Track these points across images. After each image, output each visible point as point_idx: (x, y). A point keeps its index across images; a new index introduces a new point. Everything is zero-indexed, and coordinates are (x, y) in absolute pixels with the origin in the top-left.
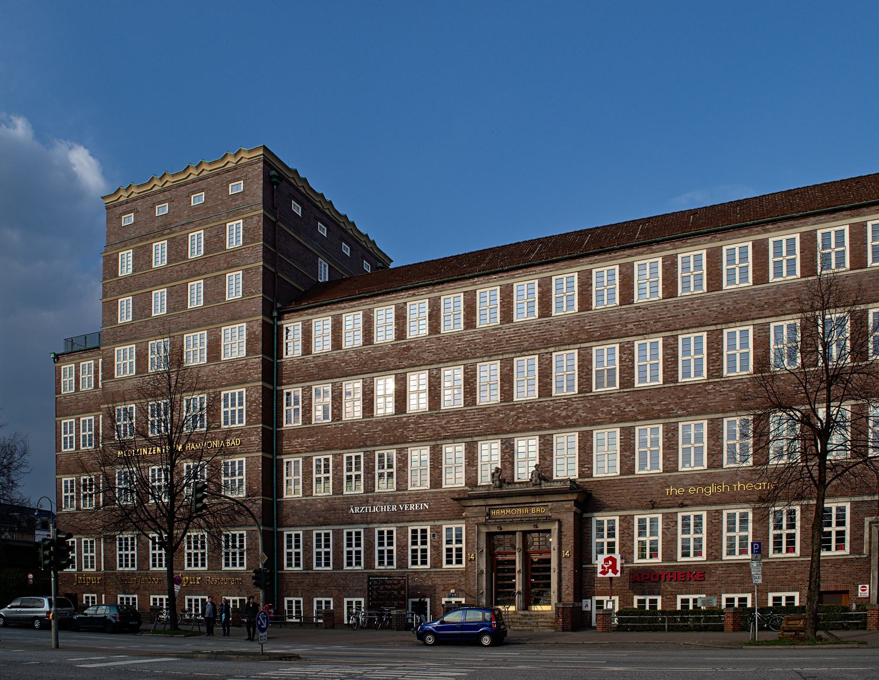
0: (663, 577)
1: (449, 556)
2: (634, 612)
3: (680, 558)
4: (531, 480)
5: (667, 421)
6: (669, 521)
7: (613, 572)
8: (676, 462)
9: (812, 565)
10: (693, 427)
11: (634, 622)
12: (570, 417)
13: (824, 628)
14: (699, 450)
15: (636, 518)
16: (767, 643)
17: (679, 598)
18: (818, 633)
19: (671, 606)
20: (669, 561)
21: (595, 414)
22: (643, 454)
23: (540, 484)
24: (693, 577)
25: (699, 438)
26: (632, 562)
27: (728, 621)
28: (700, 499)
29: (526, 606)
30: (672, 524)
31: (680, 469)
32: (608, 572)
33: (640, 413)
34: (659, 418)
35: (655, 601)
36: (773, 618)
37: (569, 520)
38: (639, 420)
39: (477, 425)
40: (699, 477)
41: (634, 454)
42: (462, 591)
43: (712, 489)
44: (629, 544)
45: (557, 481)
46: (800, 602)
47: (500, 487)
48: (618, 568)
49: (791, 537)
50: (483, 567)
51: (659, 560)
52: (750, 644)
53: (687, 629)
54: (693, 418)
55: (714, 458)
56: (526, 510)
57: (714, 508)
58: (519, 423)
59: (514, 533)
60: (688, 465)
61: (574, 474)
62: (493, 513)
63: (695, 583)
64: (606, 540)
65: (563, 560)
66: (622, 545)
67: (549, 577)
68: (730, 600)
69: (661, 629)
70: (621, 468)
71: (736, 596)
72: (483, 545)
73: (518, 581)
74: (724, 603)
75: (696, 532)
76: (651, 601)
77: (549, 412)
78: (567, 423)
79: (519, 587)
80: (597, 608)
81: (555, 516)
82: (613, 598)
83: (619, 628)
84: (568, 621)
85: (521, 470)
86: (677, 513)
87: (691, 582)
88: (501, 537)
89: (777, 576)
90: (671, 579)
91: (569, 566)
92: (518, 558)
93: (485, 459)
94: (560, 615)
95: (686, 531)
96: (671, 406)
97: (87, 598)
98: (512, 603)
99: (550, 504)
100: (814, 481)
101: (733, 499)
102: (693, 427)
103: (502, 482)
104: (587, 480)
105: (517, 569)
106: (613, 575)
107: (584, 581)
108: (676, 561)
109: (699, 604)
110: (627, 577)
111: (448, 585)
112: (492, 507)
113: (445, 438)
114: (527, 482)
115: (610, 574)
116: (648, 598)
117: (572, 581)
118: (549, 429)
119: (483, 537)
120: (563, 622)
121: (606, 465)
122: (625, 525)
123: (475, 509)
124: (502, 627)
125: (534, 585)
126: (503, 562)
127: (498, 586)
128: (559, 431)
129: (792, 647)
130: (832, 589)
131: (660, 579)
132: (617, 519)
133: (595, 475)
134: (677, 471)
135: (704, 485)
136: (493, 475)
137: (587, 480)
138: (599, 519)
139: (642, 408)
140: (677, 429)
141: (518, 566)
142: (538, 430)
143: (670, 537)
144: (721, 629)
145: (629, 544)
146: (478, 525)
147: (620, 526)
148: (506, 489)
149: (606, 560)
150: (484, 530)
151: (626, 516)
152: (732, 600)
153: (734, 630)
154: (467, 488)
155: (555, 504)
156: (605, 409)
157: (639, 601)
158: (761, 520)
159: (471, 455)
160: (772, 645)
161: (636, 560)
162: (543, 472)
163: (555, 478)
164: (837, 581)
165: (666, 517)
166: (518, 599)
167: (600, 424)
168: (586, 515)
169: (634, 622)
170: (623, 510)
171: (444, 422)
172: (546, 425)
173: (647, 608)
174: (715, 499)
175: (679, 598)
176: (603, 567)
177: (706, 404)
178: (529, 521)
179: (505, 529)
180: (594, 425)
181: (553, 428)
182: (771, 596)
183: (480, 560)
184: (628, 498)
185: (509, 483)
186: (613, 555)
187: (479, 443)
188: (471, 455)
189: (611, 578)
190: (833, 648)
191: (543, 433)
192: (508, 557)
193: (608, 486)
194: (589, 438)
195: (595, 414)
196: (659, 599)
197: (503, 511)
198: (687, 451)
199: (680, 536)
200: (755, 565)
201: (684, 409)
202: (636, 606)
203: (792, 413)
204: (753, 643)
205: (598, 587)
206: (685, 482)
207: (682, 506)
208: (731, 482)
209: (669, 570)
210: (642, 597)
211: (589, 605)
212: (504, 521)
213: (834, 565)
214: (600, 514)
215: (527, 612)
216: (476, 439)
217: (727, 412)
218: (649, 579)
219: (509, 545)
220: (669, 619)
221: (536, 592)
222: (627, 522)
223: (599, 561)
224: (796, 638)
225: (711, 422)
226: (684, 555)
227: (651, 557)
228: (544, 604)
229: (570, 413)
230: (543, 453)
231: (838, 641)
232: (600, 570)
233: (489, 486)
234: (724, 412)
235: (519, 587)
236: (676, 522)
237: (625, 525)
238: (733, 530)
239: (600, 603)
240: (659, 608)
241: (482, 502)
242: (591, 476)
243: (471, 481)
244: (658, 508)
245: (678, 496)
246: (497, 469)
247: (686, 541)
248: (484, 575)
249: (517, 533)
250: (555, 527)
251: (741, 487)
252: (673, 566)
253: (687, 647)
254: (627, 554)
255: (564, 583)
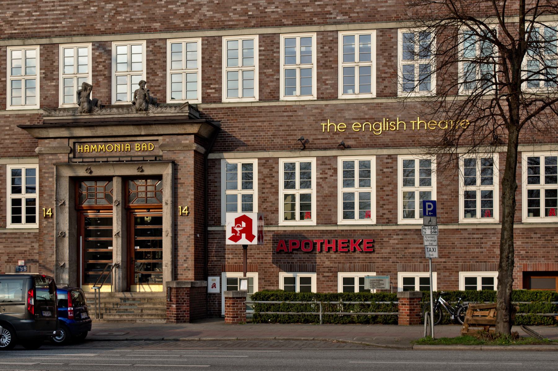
0: (318, 246)
1: (16, 211)
2: (277, 295)
3: (341, 220)
4: (134, 103)
5: (322, 28)
6: (327, 167)
7: (247, 238)
8: (335, 86)
9: (502, 234)
10: (357, 38)
11: (275, 308)
12: (190, 16)
13: (525, 323)
14: (365, 71)
15: (282, 162)
16: (447, 341)
17: (341, 276)
18: (514, 329)
19: (330, 287)
20: (326, 224)
21: (225, 14)
22: (290, 73)
23: (146, 110)
24: (357, 246)
25: (365, 54)
26: (276, 224)
27: (404, 311)
28: (367, 139)
29: (128, 285)
30: (330, 172)
31: (341, 96)
32: (240, 238)
33: (286, 15)
35: (308, 280)
36: (451, 308)
37: (188, 162)
38: (285, 25)
39: (58, 20)
41: (278, 72)
42: (35, 261)
43: (383, 126)
44: (272, 198)
45: (171, 106)
46: (318, 288)
47: (90, 111)
48: (255, 232)
49: (488, 195)
50: (65, 227)
51: (312, 222)
52: (424, 343)
53: (351, 321)
54: (357, 26)
55: (386, 83)
56: (128, 146)
57: (386, 152)
58: (118, 21)
59: (109, 179)
60: (350, 91)
61: (196, 98)
62: (78, 148)
63: (361, 256)
64: (240, 192)
65: (180, 219)
66: (262, 200)
67: (160, 244)
68: (409, 281)
69: (313, 320)
70: (260, 91)
71: (417, 276)
72: (65, 195)
73: (116, 249)
74: (400, 285)
76: (303, 280)
77: (161, 7)
78: (186, 24)
79: (117, 258)
80: (229, 289)
81: (167, 156)
82: (249, 275)
83: (258, 319)
84: (185, 307)
85: (121, 89)
86: (336, 157)
87: (357, 254)
88: (93, 184)
89: (458, 250)
90: (329, 249)
91: (187, 227)
92: (116, 215)
93: (70, 70)
94: (174, 299)
95: (348, 183)
96: (329, 8)
98: (107, 280)
99: (160, 138)
100: (505, 120)
101: (412, 141)
102: (357, 38)
103: (93, 105)
104: (213, 106)
105: (115, 231)
106: (247, 242)
107: (208, 253)
108: (336, 224)
109: (367, 286)
110: (270, 245)
111: (15, 254)
112: (79, 140)
113: (11, 37)
114: (128, 106)
115: (244, 241)
116: (299, 275)
117: (192, 249)
118: (161, 31)
119: (65, 185)
120: (178, 309)
121: (240, 89)
122: (266, 171)
123: (54, 143)
124: (84, 316)
125: (140, 255)
126: (94, 222)
127: (87, 256)
128: (175, 35)
129: (479, 347)
130: (542, 269)
131: (314, 249)
132: (255, 163)
133: (224, 100)
134: (336, 98)
135: (373, 120)
136: (79, 93)
137: (213, 106)
138: (231, 161)
139: (289, 9)
140: (335, 41)
141: (116, 227)
142: (146, 32)
143: (326, 191)
144: (394, 321)
145: (272, 198)
146: (58, 165)
147: (259, 172)
148: (99, 115)
149: (238, 221)
150: (67, 173)
151: (267, 159)
152: (412, 280)
153: (411, 323)
154: (42, 112)
155: (167, 139)
156: (239, 8)
157: (287, 280)
158: (447, 169)
159: (48, 64)
160: (453, 344)
161: (282, 222)
162: (151, 94)
163: (169, 101)
164: (548, 258)
165: (321, 161)
166: (116, 274)
167: (231, 27)
168: (211, 156)
169: (275, 308)
170: (264, 149)
171: (9, 13)
172: (157, 25)
173: (298, 290)
174: (387, 139)
175: (341, 276)
176: (234, 231)
177: (374, 8)
178: (131, 162)
179: (97, 172)
180: (223, 28)
181: (168, 30)
182: (463, 276)
183: (61, 218)
184: (270, 133)
185: (102, 107)
186: (248, 214)
187: (61, 47)
188: (48, 64)
189: (245, 247)
190: (531, 350)
192: (103, 214)
193: (243, 116)
195: (225, 14)
196: (314, 277)
197: (93, 147)
198: (349, 71)
199: (341, 190)
200: (428, 231)
201: (345, 14)
202: (282, 286)
203: (475, 27)
204: (429, 341)
205: (230, 259)
206: (347, 115)
207: (343, 147)
208: (408, 119)
209: (326, 238)
210: (290, 275)
211: (216, 284)
212: (95, 162)
213: (544, 235)
214: (231, 154)
215: (128, 295)
216: (56, 40)
217: (402, 21)
218: (299, 249)
219: (101, 195)
220: (324, 306)
221: (142, 263)
222: (269, 167)
223: (229, 220)
224: (486, 335)
225: (382, 33)
226: (346, 216)
227: (302, 218)
228: (155, 283)
229: (190, 11)
230: (152, 65)
231: (540, 340)
232: (229, 234)
233: (74, 109)
234: (398, 20)
235: (117, 258)
236: (336, 170)
237: (266, 171)
238: (412, 183)
239: (233, 282)
240: (314, 290)
241: (64, 133)
242: (219, 100)
243: (50, 103)
244: (311, 149)
245: (337, 133)
246: (85, 86)
247: (348, 196)
248: (67, 240)
249: (115, 179)
250: (167, 172)
251: (422, 126)
252: (331, 232)
253: (341, 345)
254: (268, 214)
255: (181, 253)
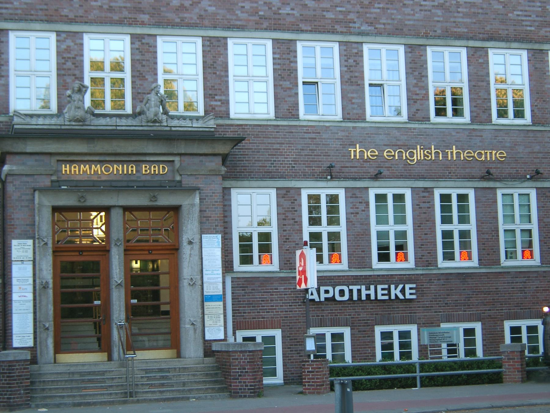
15: (304, 194)
34: (333, 32)
38: (302, 31)
40: (397, 134)
70: (276, 107)
75: (396, 222)
78: (182, 20)
86: (495, 189)
96: (352, 16)
97: (320, 338)
99: (177, 159)
121: (251, 99)
135: (407, 147)
142: (130, 25)
167: (241, 28)
181: (158, 24)
191: (139, 31)
193: (257, 136)
194: (221, 49)
201: (371, 24)
207: (377, 177)
230: (139, 67)
236: (367, 204)
245: (368, 160)
248: (51, 292)
